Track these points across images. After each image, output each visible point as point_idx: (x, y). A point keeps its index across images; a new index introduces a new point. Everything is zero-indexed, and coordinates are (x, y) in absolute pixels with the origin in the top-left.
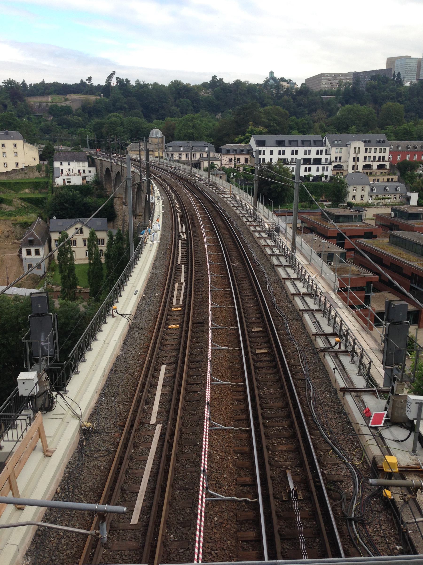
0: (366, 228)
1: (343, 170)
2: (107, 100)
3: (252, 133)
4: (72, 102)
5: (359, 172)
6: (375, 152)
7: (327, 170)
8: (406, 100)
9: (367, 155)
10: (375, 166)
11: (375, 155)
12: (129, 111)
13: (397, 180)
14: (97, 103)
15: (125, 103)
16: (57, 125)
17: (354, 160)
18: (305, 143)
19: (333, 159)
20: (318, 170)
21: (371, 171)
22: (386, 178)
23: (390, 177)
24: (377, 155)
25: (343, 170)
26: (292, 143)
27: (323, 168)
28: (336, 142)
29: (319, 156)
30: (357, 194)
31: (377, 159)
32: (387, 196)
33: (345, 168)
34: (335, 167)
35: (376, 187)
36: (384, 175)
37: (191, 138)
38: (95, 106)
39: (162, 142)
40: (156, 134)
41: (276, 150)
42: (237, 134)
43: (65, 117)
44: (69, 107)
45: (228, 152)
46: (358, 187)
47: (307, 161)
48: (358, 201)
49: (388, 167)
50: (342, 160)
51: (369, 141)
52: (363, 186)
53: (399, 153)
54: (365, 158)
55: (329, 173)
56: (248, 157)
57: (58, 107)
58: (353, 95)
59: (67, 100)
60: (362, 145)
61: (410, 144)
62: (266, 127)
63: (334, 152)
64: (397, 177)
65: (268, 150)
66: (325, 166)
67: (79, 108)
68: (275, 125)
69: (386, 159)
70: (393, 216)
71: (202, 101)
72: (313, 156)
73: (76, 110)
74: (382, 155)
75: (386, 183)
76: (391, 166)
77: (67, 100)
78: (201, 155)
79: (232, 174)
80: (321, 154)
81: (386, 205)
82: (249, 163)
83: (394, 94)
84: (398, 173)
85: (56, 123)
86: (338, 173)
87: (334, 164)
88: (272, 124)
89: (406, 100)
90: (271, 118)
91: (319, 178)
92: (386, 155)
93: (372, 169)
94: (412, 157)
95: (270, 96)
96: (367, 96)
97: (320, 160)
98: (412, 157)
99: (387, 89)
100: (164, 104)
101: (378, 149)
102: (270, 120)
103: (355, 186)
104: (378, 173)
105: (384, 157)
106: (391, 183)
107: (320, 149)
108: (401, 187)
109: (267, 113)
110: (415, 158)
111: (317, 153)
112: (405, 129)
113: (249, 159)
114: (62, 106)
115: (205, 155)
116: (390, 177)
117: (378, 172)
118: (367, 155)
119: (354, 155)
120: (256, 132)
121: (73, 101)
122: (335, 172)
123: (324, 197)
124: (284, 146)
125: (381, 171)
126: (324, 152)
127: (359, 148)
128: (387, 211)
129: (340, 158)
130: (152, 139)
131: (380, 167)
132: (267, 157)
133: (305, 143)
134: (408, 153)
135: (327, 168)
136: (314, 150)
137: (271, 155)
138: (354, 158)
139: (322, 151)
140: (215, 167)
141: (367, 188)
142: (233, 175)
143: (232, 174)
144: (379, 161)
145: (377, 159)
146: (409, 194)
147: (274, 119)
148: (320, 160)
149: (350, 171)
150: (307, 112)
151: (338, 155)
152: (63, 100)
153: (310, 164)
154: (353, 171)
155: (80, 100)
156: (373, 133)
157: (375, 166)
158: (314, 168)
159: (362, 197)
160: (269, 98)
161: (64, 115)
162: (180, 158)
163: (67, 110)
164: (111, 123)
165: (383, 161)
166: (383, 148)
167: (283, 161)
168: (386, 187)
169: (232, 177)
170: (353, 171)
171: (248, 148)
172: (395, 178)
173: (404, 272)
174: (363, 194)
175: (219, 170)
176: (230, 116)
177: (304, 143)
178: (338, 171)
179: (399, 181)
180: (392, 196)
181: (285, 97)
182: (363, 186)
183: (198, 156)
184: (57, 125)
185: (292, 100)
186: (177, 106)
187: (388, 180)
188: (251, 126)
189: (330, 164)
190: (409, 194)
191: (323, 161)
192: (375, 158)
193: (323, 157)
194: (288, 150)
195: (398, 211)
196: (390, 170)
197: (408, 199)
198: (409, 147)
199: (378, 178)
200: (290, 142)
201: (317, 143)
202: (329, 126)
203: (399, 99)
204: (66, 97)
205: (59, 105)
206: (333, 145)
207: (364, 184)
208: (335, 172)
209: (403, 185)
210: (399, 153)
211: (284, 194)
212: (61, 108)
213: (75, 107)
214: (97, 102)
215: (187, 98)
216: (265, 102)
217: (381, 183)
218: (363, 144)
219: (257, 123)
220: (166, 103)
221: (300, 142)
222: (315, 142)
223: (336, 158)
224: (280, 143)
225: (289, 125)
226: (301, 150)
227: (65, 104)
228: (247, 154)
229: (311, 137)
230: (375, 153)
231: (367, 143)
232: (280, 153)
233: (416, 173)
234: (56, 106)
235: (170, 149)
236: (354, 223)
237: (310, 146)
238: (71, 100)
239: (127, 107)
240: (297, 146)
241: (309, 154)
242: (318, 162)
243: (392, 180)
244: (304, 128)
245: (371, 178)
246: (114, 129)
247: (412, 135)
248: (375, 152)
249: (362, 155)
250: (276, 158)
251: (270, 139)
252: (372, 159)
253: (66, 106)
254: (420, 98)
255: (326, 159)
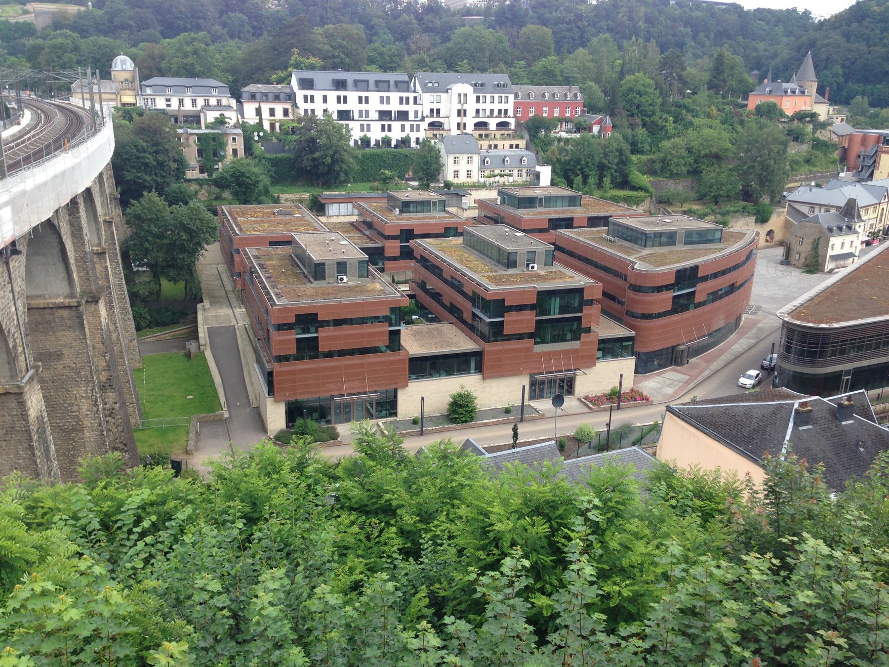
0: (447, 221)
1: (443, 129)
2: (99, 13)
3: (298, 66)
4: (36, 17)
5: (466, 134)
6: (493, 102)
7: (418, 130)
8: (589, 25)
9: (480, 106)
10: (493, 123)
11: (492, 106)
12: (139, 31)
13: (524, 147)
14: (80, 18)
15: (131, 18)
16: (7, 54)
17: (459, 114)
18: (380, 84)
19: (427, 112)
20: (403, 128)
21: (487, 132)
22: (507, 143)
23: (514, 142)
24: (496, 107)
25: (443, 129)
26: (359, 85)
27: (412, 126)
28: (430, 85)
29: (404, 108)
30: (458, 168)
31: (496, 113)
32: (507, 172)
33: (446, 127)
34: (431, 125)
35: (490, 157)
36: (504, 139)
37: (190, 73)
38: (75, 22)
39: (134, 78)
40: (123, 65)
41: (332, 95)
42: (274, 69)
43: (22, 41)
44: (30, 24)
45: (253, 97)
46: (460, 156)
47: (384, 115)
48: (462, 179)
49: (513, 127)
50: (441, 115)
51: (482, 85)
52: (470, 155)
53: (531, 105)
54: (477, 111)
55: (422, 135)
56: (288, 106)
57: (10, 24)
58: (510, 16)
59: (26, 12)
60: (467, 89)
61: (548, 90)
62: (324, 58)
63: (428, 101)
64: (524, 142)
65: (318, 95)
66: (415, 123)
67: (48, 26)
68: (343, 56)
69: (511, 113)
70: (499, 203)
71: (268, 18)
72: (394, 106)
73: (44, 29)
74: (503, 107)
75: (507, 152)
76: (518, 124)
77: (26, 12)
78: (207, 102)
79: (256, 134)
80: (407, 103)
81: (490, 187)
82: (291, 117)
83: (571, 16)
84: (527, 136)
85: (5, 51)
86: (435, 135)
87: (429, 120)
88: (337, 54)
89: (589, 25)
90: (334, 44)
91: (405, 142)
92: (510, 107)
93: (488, 129)
94: (551, 111)
95: (380, 13)
96: (531, 18)
97: (407, 113)
98: (551, 111)
99: (562, 8)
100: (201, 21)
101: (496, 96)
102: (334, 48)
103: (457, 155)
104: (498, 136)
105: (506, 111)
106: (512, 149)
107: (405, 95)
108: (528, 157)
109: (329, 36)
110: (556, 113)
111: (401, 103)
112: (545, 67)
113: (290, 110)
114: (17, 23)
115: (213, 102)
116: (514, 142)
117: (498, 134)
118: (480, 106)
119: (459, 107)
120: (305, 66)
121: (38, 14)
122: (430, 134)
123: (411, 174)
124: (346, 90)
125: (502, 132)
126: (411, 101)
127: (465, 95)
128: (493, 195)
129: (438, 111)
130: (116, 73)
131: (502, 125)
132: (318, 108)
133: (400, 85)
134: (546, 105)
135: (418, 126)
136: (395, 96)
137: (322, 103)
138: (459, 111)
139: (407, 98)
140: (226, 123)
141: (476, 159)
142: (258, 135)
143: (256, 134)
144: (499, 116)
145: (496, 113)
146: (538, 168)
147: (340, 46)
148: (407, 113)
149: (455, 132)
150: (440, 41)
151: (435, 106)
152: (20, 12)
153: (390, 120)
154: (459, 132)
155: (49, 13)
156: (495, 72)
157: (493, 123)
158: (396, 125)
159: (469, 175)
160: (378, 17)
161: (20, 38)
162: (169, 105)
163: (27, 30)
164: (55, 47)
165: (506, 117)
166: (503, 95)
167: (345, 115)
168: (505, 157)
169: (256, 138)
170: (459, 132)
171: (287, 91)
172: (522, 143)
173: (465, 289)
174: (469, 167)
175: (235, 127)
176: (263, 42)
177: (380, 86)
178: (435, 132)
179: (527, 148)
180: (516, 172)
181: (405, 17)
182: (470, 155)
183: (200, 102)
184: (7, 54)
185: (415, 21)
186: (224, 25)
187: (511, 146)
188: (296, 56)
189: (423, 120)
190: (538, 168)
191: (411, 116)
192: (492, 111)
193: (411, 108)
194: (353, 96)
195: (507, 194)
196: (515, 131)
197: (537, 176)
198: (547, 94)
199: (496, 142)
200: (356, 82)
201: (401, 86)
202: (434, 60)
203: (579, 24)
204: (25, 8)
205: (13, 21)
206: (426, 90)
207: (470, 151)
208: (430, 134)
209: (531, 154)
210: (531, 105)
211: (337, 168)
212: (15, 26)
213: (40, 24)
214: (79, 15)
215: (242, 11)
216: (372, 23)
217: (500, 152)
218: (471, 89)
219: (306, 51)
220: (205, 19)
221: (392, 84)
222: (397, 83)
223: (432, 111)
224: (340, 85)
225: (369, 57)
226: (374, 96)
227: (22, 19)
228: (286, 101)
229: (392, 77)
230: (493, 104)
231: (479, 87)
232: (339, 101)
233: (553, 135)
234: (7, 21)
235: (149, 91)
236: (433, 214)
237: (389, 91)
238: (34, 12)
239: (134, 25)
240: (367, 90)
241: (388, 102)
242: (403, 116)
243: (517, 146)
244: (392, 62)
245: (485, 143)
246: (59, 57)
247: (554, 76)
248: (493, 102)
249: (471, 106)
250: (334, 107)
251: (323, 77)
252: (488, 113)
253: (25, 23)
254: (610, 22)
255: (416, 112)
